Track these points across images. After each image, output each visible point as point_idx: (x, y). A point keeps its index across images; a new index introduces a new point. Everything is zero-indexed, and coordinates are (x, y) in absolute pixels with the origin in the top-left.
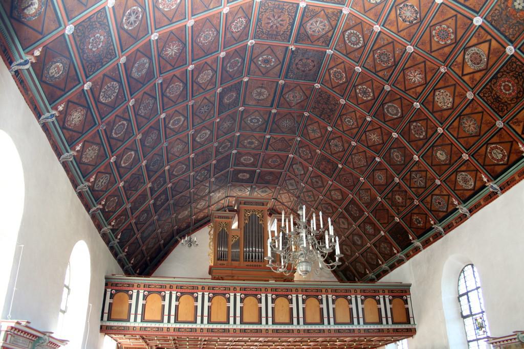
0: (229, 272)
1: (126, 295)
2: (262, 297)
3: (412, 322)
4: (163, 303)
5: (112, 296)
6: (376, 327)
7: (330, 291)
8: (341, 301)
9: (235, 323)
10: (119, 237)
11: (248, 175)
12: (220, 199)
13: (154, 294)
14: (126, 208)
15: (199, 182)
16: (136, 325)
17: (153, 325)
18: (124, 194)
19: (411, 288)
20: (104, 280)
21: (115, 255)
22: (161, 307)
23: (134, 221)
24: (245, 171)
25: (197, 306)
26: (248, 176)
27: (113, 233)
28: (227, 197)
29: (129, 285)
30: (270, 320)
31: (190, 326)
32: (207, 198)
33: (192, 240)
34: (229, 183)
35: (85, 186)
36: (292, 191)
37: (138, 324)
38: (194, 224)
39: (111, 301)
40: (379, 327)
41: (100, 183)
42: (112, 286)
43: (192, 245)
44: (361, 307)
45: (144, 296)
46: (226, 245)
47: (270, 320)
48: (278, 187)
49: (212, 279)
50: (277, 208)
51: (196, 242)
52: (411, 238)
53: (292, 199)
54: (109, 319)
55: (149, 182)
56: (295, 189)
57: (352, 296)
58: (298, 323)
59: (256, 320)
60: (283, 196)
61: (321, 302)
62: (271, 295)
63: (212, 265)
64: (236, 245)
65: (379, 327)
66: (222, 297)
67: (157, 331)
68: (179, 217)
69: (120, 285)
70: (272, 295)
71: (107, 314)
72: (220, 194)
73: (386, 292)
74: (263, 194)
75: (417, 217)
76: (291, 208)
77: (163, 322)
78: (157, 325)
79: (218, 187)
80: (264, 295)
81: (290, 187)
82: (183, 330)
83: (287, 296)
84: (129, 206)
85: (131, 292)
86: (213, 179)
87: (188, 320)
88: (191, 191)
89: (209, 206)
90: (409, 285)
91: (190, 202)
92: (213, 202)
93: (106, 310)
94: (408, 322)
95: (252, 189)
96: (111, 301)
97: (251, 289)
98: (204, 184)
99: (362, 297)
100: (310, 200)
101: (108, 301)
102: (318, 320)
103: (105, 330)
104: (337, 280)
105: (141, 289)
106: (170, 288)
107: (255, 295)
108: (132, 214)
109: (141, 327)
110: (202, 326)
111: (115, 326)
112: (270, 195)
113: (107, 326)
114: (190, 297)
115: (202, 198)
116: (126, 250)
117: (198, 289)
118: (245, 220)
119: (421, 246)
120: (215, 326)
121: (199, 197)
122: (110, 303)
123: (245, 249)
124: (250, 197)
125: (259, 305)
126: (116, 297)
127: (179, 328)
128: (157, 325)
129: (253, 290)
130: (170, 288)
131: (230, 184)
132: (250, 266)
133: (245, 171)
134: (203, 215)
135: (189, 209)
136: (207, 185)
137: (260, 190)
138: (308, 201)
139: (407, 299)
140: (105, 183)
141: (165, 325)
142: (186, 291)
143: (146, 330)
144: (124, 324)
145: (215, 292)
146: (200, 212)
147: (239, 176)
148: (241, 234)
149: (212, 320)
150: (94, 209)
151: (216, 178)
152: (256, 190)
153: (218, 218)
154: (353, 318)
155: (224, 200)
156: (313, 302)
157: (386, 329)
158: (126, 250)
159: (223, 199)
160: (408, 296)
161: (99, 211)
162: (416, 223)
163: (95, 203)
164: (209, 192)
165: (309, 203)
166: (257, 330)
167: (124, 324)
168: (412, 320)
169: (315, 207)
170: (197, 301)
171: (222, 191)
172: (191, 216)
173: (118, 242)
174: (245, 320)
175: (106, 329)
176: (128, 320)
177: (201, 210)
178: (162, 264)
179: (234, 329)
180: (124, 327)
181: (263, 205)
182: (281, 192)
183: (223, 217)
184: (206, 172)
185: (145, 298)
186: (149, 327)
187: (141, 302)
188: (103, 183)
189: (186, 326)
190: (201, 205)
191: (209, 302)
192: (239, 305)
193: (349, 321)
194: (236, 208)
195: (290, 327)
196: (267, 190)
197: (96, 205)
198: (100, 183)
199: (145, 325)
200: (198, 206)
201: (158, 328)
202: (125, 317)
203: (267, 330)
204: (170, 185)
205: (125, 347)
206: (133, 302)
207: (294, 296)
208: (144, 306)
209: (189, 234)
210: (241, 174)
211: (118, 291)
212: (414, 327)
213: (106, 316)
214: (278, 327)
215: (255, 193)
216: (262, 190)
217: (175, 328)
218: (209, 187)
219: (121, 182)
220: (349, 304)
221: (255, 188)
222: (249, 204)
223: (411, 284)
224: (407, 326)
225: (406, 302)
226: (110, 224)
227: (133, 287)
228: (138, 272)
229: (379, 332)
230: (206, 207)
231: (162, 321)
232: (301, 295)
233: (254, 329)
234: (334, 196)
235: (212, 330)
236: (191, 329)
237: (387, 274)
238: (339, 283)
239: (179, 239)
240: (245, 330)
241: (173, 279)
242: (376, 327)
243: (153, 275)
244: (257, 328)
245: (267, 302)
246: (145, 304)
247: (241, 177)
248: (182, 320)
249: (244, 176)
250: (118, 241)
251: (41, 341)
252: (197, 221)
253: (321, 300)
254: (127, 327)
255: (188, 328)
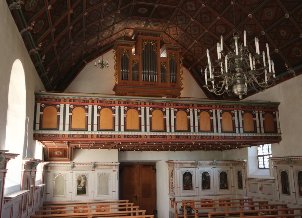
0: (131, 89)
1: (54, 108)
2: (142, 110)
3: (279, 132)
4: (86, 115)
5: (42, 109)
6: (252, 135)
7: (218, 106)
8: (227, 114)
9: (146, 130)
10: (44, 58)
11: (146, 10)
12: (120, 30)
13: (78, 108)
14: (50, 33)
15: (108, 13)
16: (65, 133)
17: (80, 133)
18: (50, 18)
19: (279, 105)
20: (34, 96)
21: (40, 74)
22: (85, 118)
23: (56, 44)
24: (144, 6)
25: (115, 117)
26: (146, 10)
27: (39, 54)
28: (125, 28)
29: (56, 100)
30: (173, 128)
31: (110, 133)
32: (111, 29)
33: (104, 62)
34: (129, 16)
35: (18, 4)
36: (180, 26)
37: (67, 132)
38: (98, 50)
39: (42, 113)
40: (255, 135)
41: (30, 4)
42: (41, 100)
43: (104, 66)
44: (149, 117)
45: (70, 109)
46: (128, 68)
47: (173, 128)
48: (168, 22)
49: (116, 95)
50: (164, 39)
51: (107, 64)
52: (287, 66)
53: (179, 32)
54: (41, 128)
55: (71, 9)
56: (184, 24)
57: (190, 109)
58: (194, 131)
59: (162, 128)
60: (171, 30)
61: (211, 115)
62: (96, 106)
63: (117, 83)
64: (136, 68)
65: (255, 135)
66: (135, 110)
67: (83, 137)
68: (88, 44)
69: (48, 100)
70: (174, 109)
71: (39, 125)
72: (121, 26)
73: (240, 107)
74: (155, 28)
75: (298, 49)
76: (176, 39)
77: (87, 130)
78: (83, 133)
79: (121, 19)
80: (143, 108)
81: (179, 22)
82: (104, 136)
83: (186, 109)
84: (54, 30)
85: (164, 109)
86: (119, 12)
87: (108, 129)
88: (102, 21)
89: (111, 36)
90: (279, 104)
91: (98, 31)
92: (115, 32)
93: (38, 121)
94: (276, 132)
95: (147, 23)
96: (42, 113)
97: (157, 104)
98: (112, 15)
99: (242, 111)
100: (195, 33)
101: (39, 113)
102: (209, 129)
103: (37, 137)
104: (207, 98)
105: (67, 103)
106: (92, 102)
107: (208, 110)
108: (55, 38)
109: (69, 135)
110: (120, 133)
111: (47, 134)
112: (160, 28)
113: (39, 134)
114: (109, 110)
115: (108, 28)
116: (48, 70)
117: (88, 102)
118: (142, 47)
119: (294, 73)
120: (130, 133)
121: (106, 27)
122: (40, 115)
123: (143, 71)
124: (145, 28)
125: (188, 117)
126: (45, 110)
127: (101, 135)
128: (83, 133)
129: (159, 104)
130: (64, 101)
131: (131, 17)
132: (147, 84)
133: (144, 6)
134: (105, 43)
135: (96, 38)
136: (113, 16)
137: (153, 24)
138: (193, 34)
139: (212, 112)
140: (34, 4)
141: (89, 132)
142: (105, 105)
143: (74, 137)
144: (54, 132)
145: (129, 105)
146: (104, 40)
147: (139, 10)
148: (139, 59)
149: (127, 128)
150: (25, 30)
151: (121, 11)
152: (150, 23)
153: (121, 45)
154: (235, 128)
155: (122, 31)
156: (205, 114)
157: (259, 136)
158: (48, 70)
159: (123, 30)
160: (276, 112)
161: (29, 33)
162: (295, 54)
163: (26, 24)
164: (114, 24)
165: (193, 36)
166: (163, 136)
167: (54, 132)
168: (278, 130)
169: (198, 39)
170: (115, 113)
171: (123, 23)
172: (97, 43)
173: (43, 63)
174: (153, 128)
175: (39, 136)
176: (58, 129)
177: (105, 39)
178: (73, 82)
179: (145, 135)
180: (54, 134)
181: (157, 36)
182: (170, 26)
183: (126, 45)
184: (115, 4)
185: (71, 110)
186: (76, 135)
187: (68, 114)
188: (33, 5)
189: (107, 133)
190: (105, 34)
191: (124, 114)
192: (148, 116)
193: (231, 129)
194: (133, 38)
195: (189, 134)
196: (159, 24)
197: (26, 25)
198: (30, 4)
199: (72, 133)
200: (104, 35)
201: (83, 135)
202: (55, 127)
203: (171, 136)
204: (86, 14)
205: (49, 148)
206: (61, 114)
207: (143, 108)
208: (70, 117)
209: (101, 57)
210: (141, 9)
211: (46, 105)
212: (280, 135)
213: (38, 126)
214: (180, 134)
215: (149, 27)
216: (155, 23)
217: (97, 135)
218: (115, 18)
219: (49, 5)
220: (232, 117)
221: (150, 22)
222: (145, 35)
223: (280, 103)
224: (275, 135)
225: (275, 116)
226: (37, 46)
227: (60, 101)
228: (55, 88)
229: (254, 138)
230: (108, 36)
231: (86, 129)
232: (173, 109)
233: (160, 136)
234: (218, 30)
235: (128, 136)
236: (111, 135)
237: (255, 94)
238: (208, 100)
239: (86, 62)
240: (154, 136)
241: (93, 95)
242: (252, 135)
243: (65, 91)
244: (163, 134)
245: (170, 114)
246: (99, 117)
247: (140, 12)
248: (103, 128)
249: (143, 10)
250: (43, 61)
251: (34, 164)
252: (100, 48)
253: (212, 113)
254: (57, 134)
255: (108, 135)
